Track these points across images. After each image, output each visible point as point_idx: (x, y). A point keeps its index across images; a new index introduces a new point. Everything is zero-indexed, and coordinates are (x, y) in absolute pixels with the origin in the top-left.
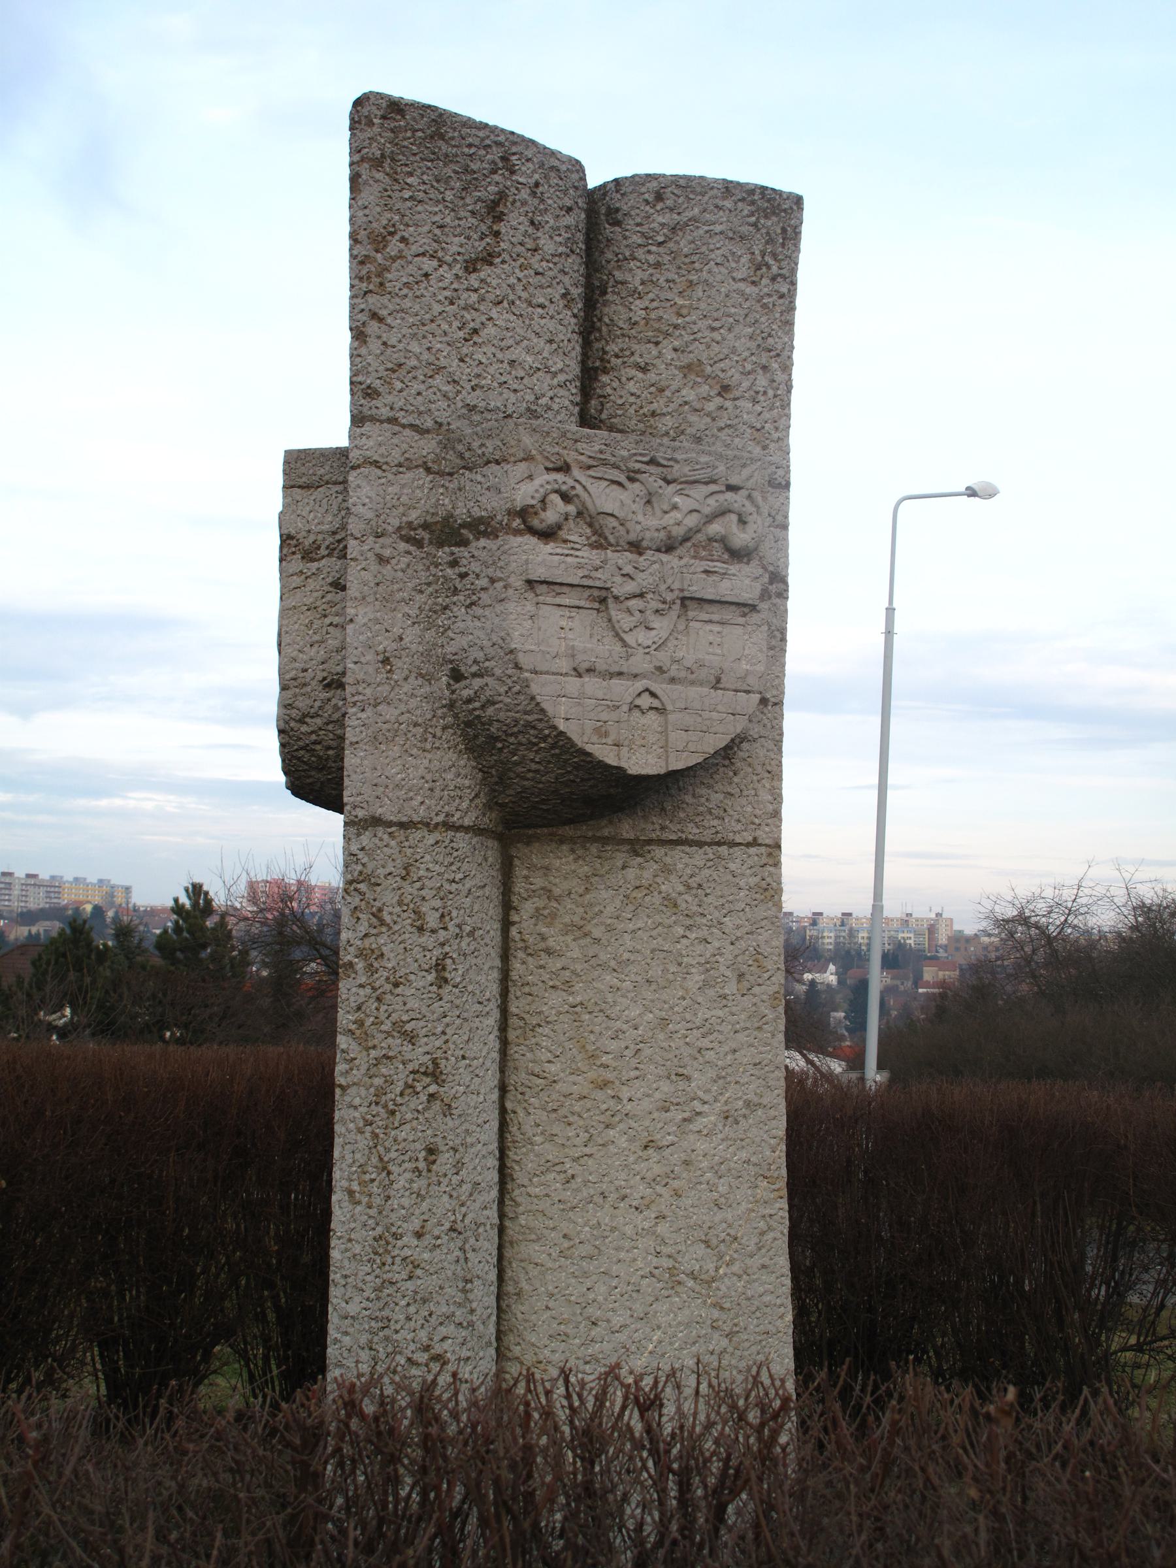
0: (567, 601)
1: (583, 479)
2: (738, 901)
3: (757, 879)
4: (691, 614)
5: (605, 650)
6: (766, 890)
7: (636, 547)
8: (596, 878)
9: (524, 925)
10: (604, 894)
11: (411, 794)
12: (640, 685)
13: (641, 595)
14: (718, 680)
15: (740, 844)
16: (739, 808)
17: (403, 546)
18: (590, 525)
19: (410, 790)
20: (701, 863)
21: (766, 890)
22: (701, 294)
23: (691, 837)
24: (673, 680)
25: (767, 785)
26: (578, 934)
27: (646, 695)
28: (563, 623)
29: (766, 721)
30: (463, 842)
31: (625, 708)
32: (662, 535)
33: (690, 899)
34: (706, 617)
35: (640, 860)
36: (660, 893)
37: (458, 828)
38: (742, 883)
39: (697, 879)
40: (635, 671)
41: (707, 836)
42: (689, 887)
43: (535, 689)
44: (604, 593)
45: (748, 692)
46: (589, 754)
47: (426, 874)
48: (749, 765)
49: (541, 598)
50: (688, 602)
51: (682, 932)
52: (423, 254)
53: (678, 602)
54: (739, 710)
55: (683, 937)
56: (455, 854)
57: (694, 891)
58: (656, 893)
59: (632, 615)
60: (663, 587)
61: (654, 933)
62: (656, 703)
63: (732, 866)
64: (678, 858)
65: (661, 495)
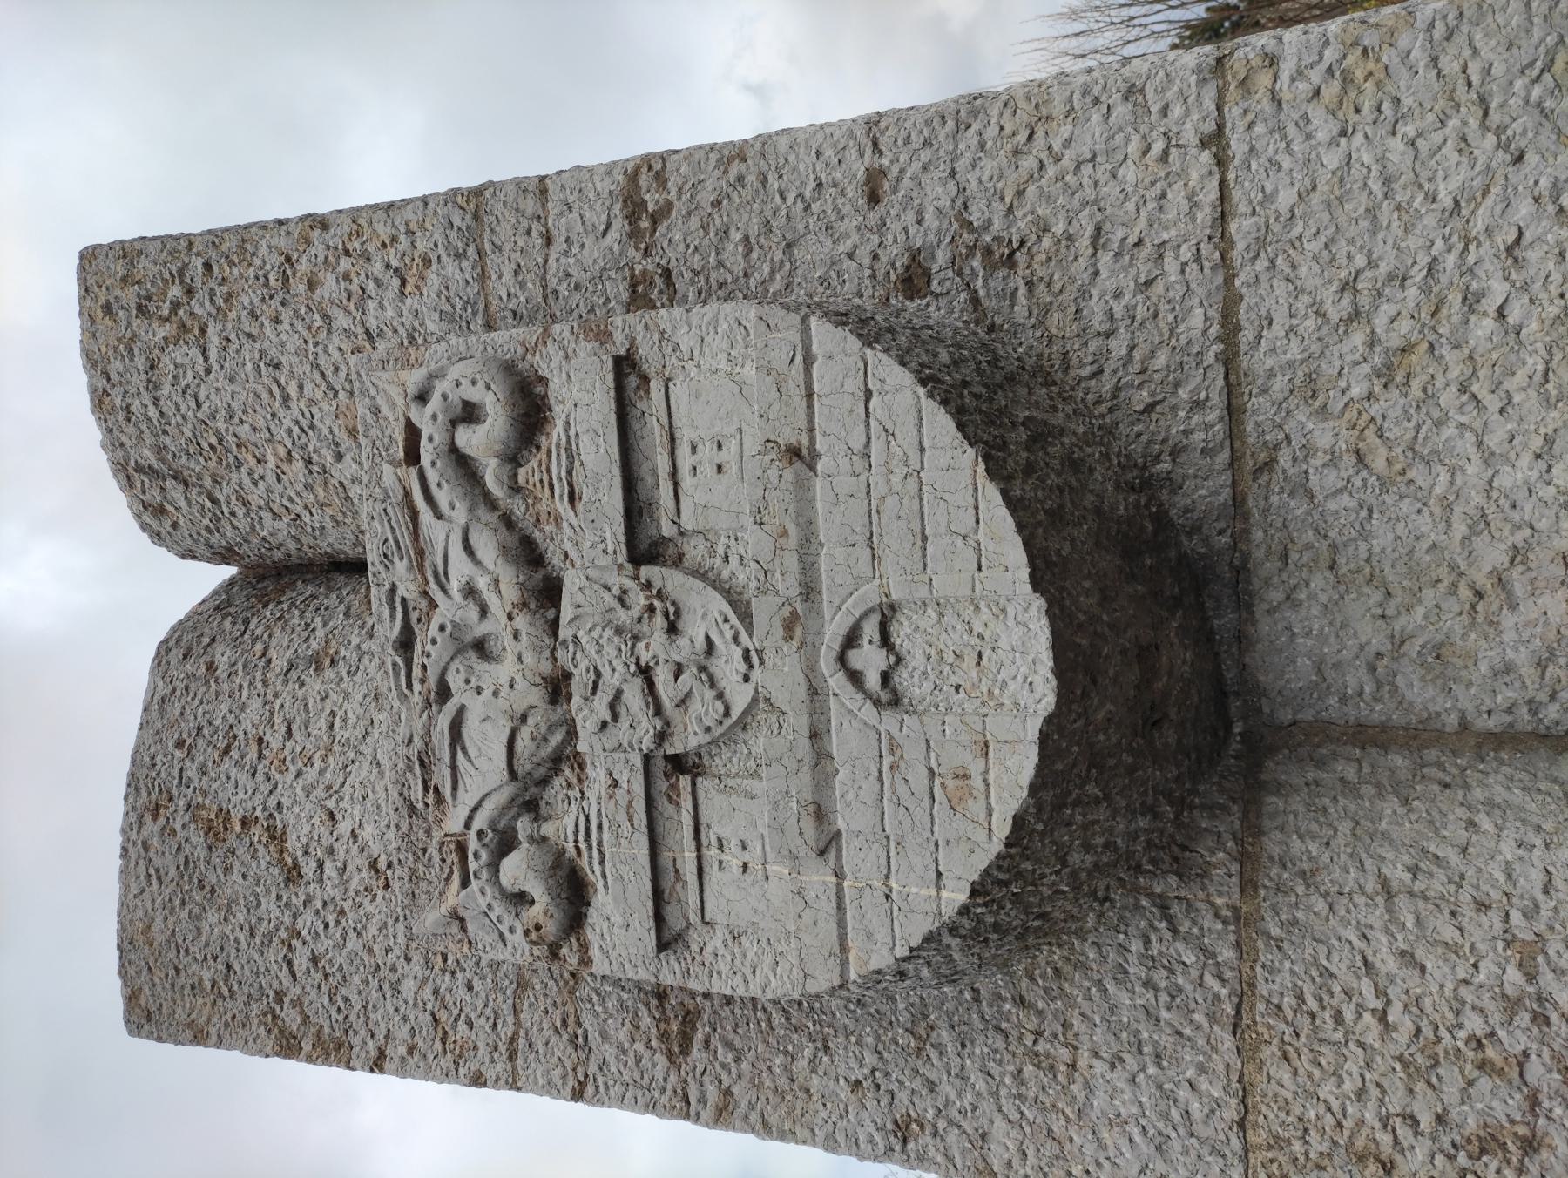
0: (690, 855)
1: (463, 813)
2: (1382, 160)
3: (1317, 115)
4: (667, 530)
5: (777, 741)
6: (1347, 79)
7: (557, 687)
8: (1342, 560)
9: (1467, 704)
10: (1382, 539)
11: (1175, 1114)
12: (836, 681)
13: (645, 672)
14: (794, 453)
15: (1223, 184)
16: (1130, 206)
17: (697, 1054)
18: (544, 782)
19: (1166, 1117)
20: (1281, 288)
21: (1347, 79)
22: (246, 427)
23: (1214, 330)
24: (809, 591)
25: (1066, 131)
26: (1493, 601)
27: (856, 659)
28: (735, 864)
29: (916, 166)
30: (1281, 978)
31: (889, 721)
32: (521, 621)
33: (1387, 309)
34: (665, 493)
35: (1284, 458)
36: (1370, 396)
37: (1245, 994)
38: (1332, 159)
39: (1328, 294)
40: (802, 692)
41: (1204, 283)
42: (1355, 315)
43: (881, 959)
44: (659, 765)
45: (809, 360)
46: (1019, 821)
47: (1372, 1105)
48: (1020, 193)
49: (694, 918)
50: (643, 546)
51: (1489, 324)
52: (290, 963)
53: (645, 571)
54: (854, 384)
55: (1501, 314)
56: (1312, 1004)
57: (1364, 301)
58: (1375, 409)
59: (688, 695)
60: (623, 616)
61: (1492, 403)
62: (871, 629)
63: (1286, 198)
64: (1271, 356)
65: (455, 625)
